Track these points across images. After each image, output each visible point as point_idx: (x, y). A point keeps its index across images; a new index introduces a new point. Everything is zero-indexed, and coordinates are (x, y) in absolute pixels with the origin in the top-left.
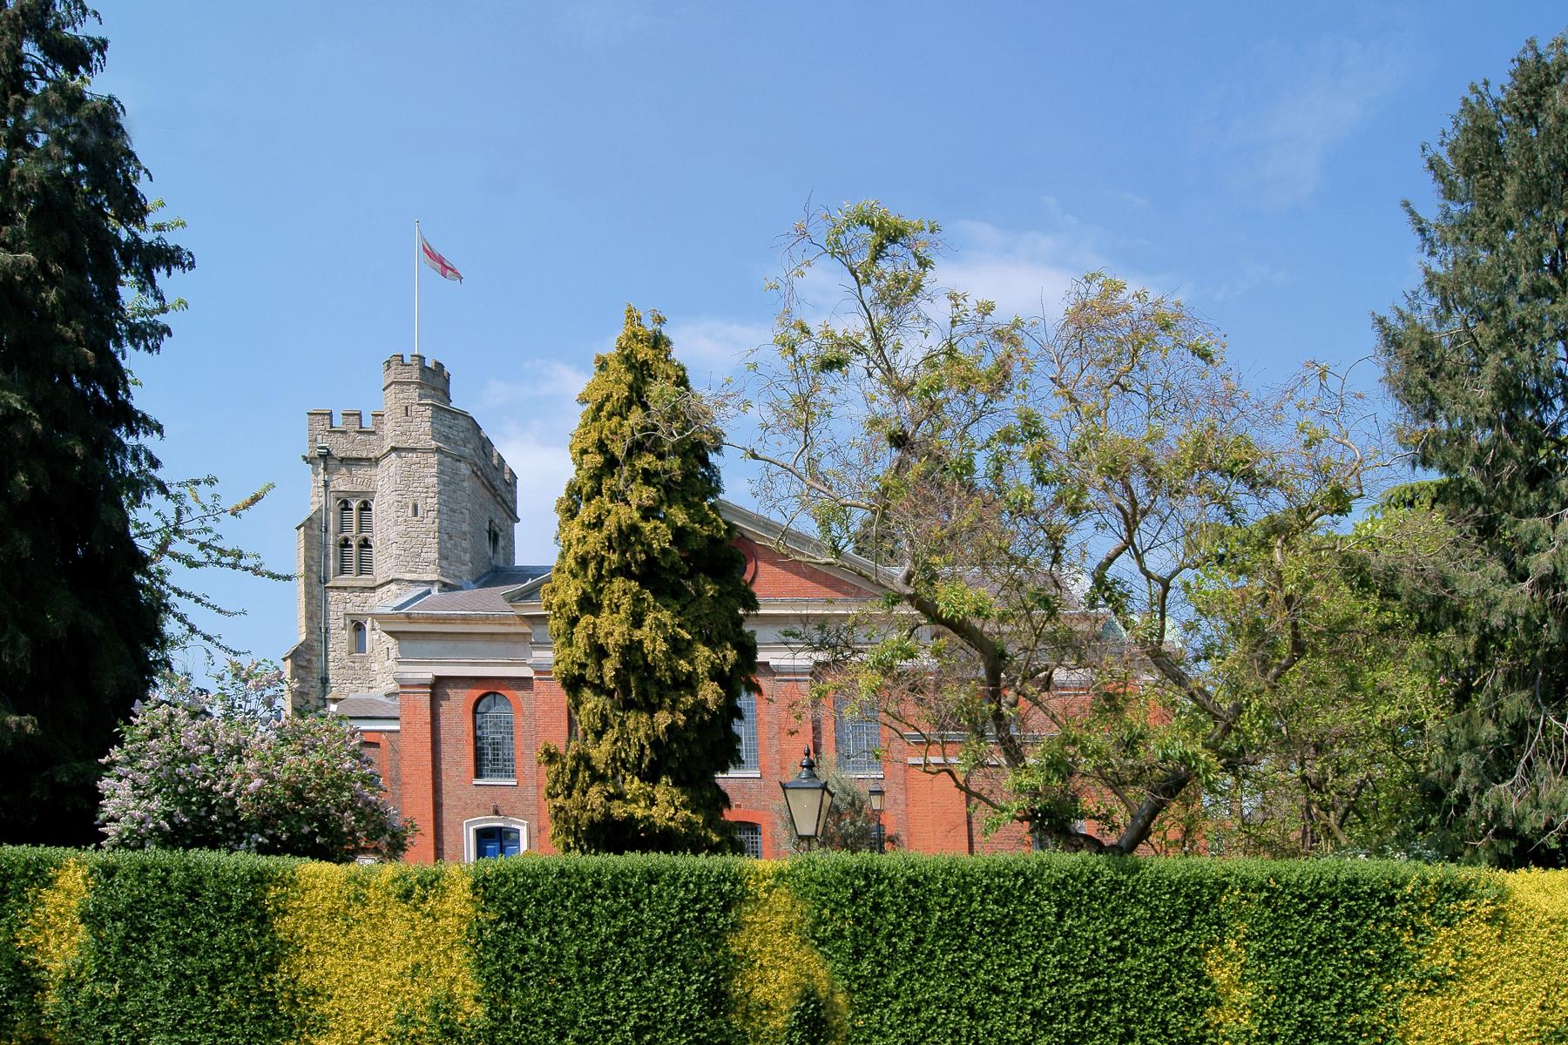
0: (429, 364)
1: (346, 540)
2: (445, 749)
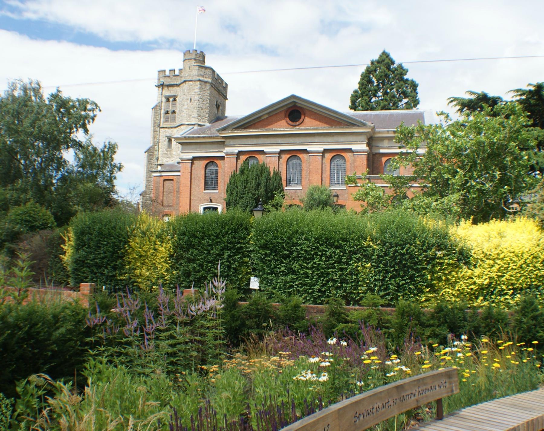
0: (198, 52)
1: (168, 111)
2: (189, 203)
